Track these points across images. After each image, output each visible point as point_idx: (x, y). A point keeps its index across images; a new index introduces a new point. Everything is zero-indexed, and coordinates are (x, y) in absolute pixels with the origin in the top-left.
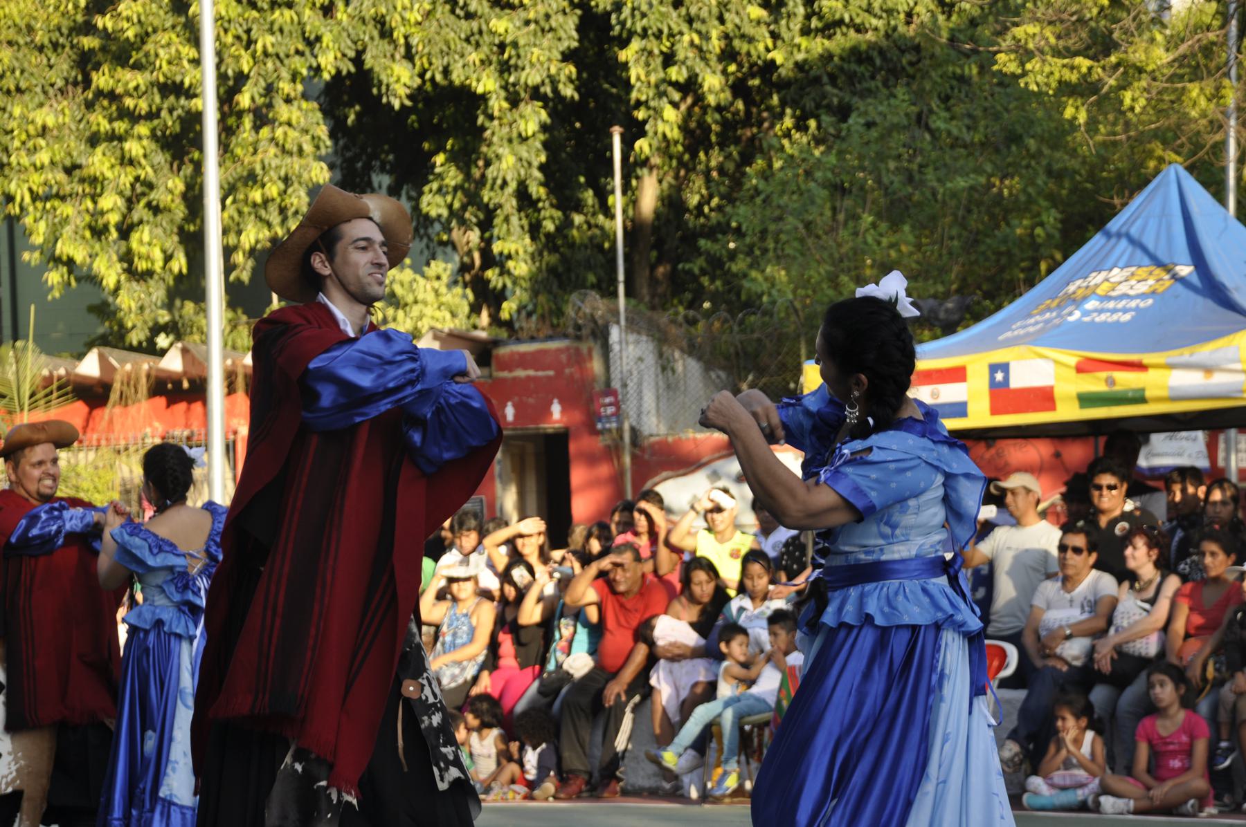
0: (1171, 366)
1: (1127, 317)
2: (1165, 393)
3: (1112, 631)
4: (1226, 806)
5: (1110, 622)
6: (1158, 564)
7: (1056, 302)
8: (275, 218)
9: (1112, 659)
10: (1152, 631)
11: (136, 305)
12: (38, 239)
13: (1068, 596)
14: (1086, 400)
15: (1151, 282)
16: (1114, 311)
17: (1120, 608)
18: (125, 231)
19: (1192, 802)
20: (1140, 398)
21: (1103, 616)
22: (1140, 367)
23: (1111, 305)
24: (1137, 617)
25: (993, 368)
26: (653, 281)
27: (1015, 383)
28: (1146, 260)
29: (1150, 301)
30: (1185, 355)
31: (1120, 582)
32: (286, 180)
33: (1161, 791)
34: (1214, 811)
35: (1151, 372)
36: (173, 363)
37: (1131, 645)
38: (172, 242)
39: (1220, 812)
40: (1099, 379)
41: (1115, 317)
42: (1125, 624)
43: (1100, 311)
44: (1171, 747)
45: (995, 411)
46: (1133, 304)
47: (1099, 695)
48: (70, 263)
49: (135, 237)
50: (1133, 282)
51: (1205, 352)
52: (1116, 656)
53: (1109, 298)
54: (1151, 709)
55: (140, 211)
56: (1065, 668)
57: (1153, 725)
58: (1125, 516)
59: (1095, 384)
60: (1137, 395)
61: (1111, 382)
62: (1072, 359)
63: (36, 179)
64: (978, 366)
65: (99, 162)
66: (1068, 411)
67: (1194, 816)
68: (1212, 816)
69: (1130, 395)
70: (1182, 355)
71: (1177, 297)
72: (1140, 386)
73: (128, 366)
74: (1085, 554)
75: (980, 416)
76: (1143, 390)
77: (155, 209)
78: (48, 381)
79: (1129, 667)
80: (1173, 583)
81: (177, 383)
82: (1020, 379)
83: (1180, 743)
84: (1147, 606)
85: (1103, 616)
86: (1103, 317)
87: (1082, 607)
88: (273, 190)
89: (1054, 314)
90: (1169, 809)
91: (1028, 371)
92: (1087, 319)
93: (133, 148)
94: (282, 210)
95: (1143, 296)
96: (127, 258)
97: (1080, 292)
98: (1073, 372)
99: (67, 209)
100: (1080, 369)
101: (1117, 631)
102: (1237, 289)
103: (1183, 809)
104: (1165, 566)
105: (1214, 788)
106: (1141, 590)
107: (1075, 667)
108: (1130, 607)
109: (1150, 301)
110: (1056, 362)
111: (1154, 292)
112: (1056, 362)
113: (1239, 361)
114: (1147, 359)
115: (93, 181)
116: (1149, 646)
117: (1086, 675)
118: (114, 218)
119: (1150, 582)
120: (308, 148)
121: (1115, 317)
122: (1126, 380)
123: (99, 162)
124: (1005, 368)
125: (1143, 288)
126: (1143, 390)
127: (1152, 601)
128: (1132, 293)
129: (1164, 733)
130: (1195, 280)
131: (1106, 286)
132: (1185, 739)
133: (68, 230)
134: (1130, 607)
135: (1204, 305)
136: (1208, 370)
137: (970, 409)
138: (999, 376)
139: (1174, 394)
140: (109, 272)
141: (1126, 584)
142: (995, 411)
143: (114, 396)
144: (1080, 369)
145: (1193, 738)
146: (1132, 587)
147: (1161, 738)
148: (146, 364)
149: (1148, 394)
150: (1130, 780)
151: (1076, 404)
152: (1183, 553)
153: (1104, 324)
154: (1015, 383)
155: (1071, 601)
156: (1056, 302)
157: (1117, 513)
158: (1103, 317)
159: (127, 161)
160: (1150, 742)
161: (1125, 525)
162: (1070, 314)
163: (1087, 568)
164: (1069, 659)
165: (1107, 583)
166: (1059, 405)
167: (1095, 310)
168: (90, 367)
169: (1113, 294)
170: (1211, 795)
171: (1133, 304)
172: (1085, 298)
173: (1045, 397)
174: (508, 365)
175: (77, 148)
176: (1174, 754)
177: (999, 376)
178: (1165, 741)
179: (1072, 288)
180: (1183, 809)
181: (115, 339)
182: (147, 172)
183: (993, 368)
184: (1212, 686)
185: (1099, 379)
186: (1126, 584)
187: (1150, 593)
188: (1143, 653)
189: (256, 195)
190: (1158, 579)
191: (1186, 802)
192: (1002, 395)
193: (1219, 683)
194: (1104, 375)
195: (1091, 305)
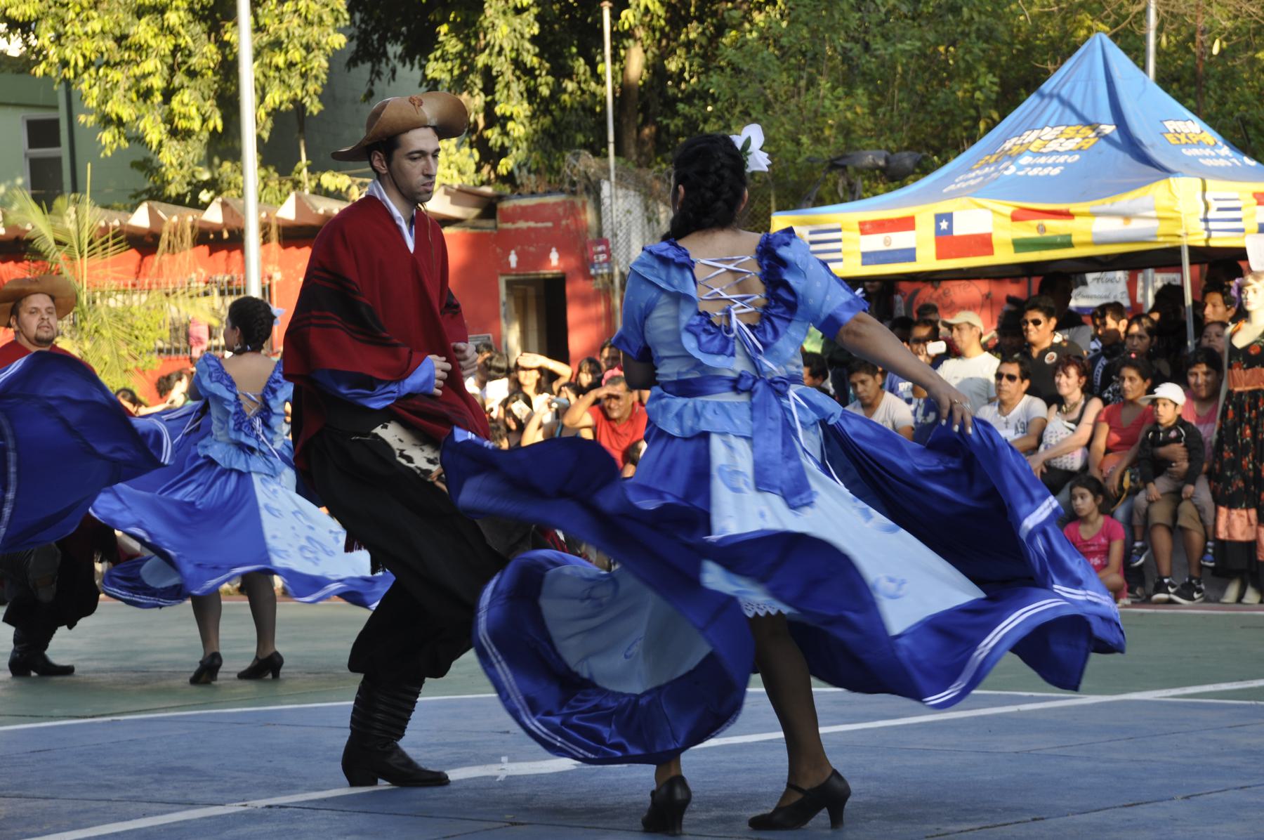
0: (1095, 214)
1: (1056, 171)
2: (1088, 238)
3: (1042, 448)
6: (1084, 390)
7: (995, 157)
8: (295, 81)
10: (1078, 447)
11: (179, 162)
12: (92, 103)
13: (1004, 419)
14: (1020, 245)
15: (1078, 139)
16: (1045, 166)
17: (1049, 428)
18: (168, 94)
20: (1069, 244)
22: (1067, 215)
23: (1043, 160)
24: (1064, 436)
25: (939, 218)
26: (640, 143)
27: (957, 232)
28: (1075, 120)
29: (1077, 157)
31: (1049, 406)
32: (308, 48)
34: (1127, 601)
35: (1077, 219)
36: (214, 215)
38: (209, 106)
40: (1031, 226)
41: (1046, 171)
42: (1053, 442)
43: (1033, 166)
44: (1092, 548)
45: (940, 256)
46: (1062, 159)
48: (120, 122)
49: (175, 103)
50: (1062, 140)
51: (1124, 201)
53: (1042, 154)
55: (180, 78)
57: (1077, 530)
58: (1054, 347)
59: (1028, 230)
60: (1065, 240)
61: (1042, 229)
62: (1008, 208)
63: (89, 46)
64: (925, 216)
65: (143, 31)
66: (1004, 255)
68: (1126, 606)
71: (1100, 153)
72: (1068, 232)
73: (177, 219)
74: (1018, 380)
75: (927, 261)
76: (1070, 236)
77: (192, 74)
78: (105, 230)
80: (1096, 405)
81: (218, 234)
82: (962, 228)
84: (1072, 426)
86: (1035, 171)
87: (1016, 428)
88: (296, 55)
91: (972, 218)
92: (1021, 173)
93: (172, 18)
94: (304, 75)
95: (1070, 152)
96: (169, 119)
97: (1015, 149)
99: (116, 75)
100: (1015, 218)
101: (1046, 448)
102: (1152, 146)
104: (1089, 391)
106: (1066, 413)
108: (1058, 427)
109: (1077, 157)
110: (993, 211)
111: (1080, 149)
112: (993, 211)
113: (1154, 209)
114: (1073, 208)
115: (139, 48)
116: (1075, 461)
118: (157, 82)
119: (1075, 405)
120: (329, 20)
121: (1046, 171)
122: (1055, 227)
123: (143, 31)
124: (949, 217)
125: (1071, 145)
126: (1070, 236)
127: (1077, 422)
128: (1061, 149)
129: (1085, 536)
130: (1117, 137)
132: (1103, 541)
133: (118, 94)
134: (1058, 427)
136: (1127, 217)
138: (944, 225)
139: (1097, 239)
140: (154, 132)
141: (1055, 407)
142: (940, 256)
143: (163, 245)
144: (1015, 218)
145: (1110, 540)
146: (1059, 409)
148: (190, 216)
149: (1074, 239)
151: (1012, 248)
152: (1107, 380)
153: (1037, 177)
154: (957, 232)
155: (1007, 423)
156: (995, 157)
157: (1047, 344)
159: (167, 30)
161: (1054, 354)
162: (1006, 169)
163: (1020, 394)
167: (1029, 165)
168: (140, 219)
169: (1044, 150)
171: (1062, 159)
172: (1020, 154)
173: (983, 243)
174: (511, 217)
175: (124, 17)
179: (1008, 145)
181: (157, 194)
182: (186, 40)
183: (939, 218)
184: (1128, 495)
185: (1031, 226)
186: (1055, 407)
187: (1075, 415)
189: (280, 60)
190: (1083, 402)
192: (946, 242)
193: (1134, 492)
194: (1036, 222)
195: (1026, 160)
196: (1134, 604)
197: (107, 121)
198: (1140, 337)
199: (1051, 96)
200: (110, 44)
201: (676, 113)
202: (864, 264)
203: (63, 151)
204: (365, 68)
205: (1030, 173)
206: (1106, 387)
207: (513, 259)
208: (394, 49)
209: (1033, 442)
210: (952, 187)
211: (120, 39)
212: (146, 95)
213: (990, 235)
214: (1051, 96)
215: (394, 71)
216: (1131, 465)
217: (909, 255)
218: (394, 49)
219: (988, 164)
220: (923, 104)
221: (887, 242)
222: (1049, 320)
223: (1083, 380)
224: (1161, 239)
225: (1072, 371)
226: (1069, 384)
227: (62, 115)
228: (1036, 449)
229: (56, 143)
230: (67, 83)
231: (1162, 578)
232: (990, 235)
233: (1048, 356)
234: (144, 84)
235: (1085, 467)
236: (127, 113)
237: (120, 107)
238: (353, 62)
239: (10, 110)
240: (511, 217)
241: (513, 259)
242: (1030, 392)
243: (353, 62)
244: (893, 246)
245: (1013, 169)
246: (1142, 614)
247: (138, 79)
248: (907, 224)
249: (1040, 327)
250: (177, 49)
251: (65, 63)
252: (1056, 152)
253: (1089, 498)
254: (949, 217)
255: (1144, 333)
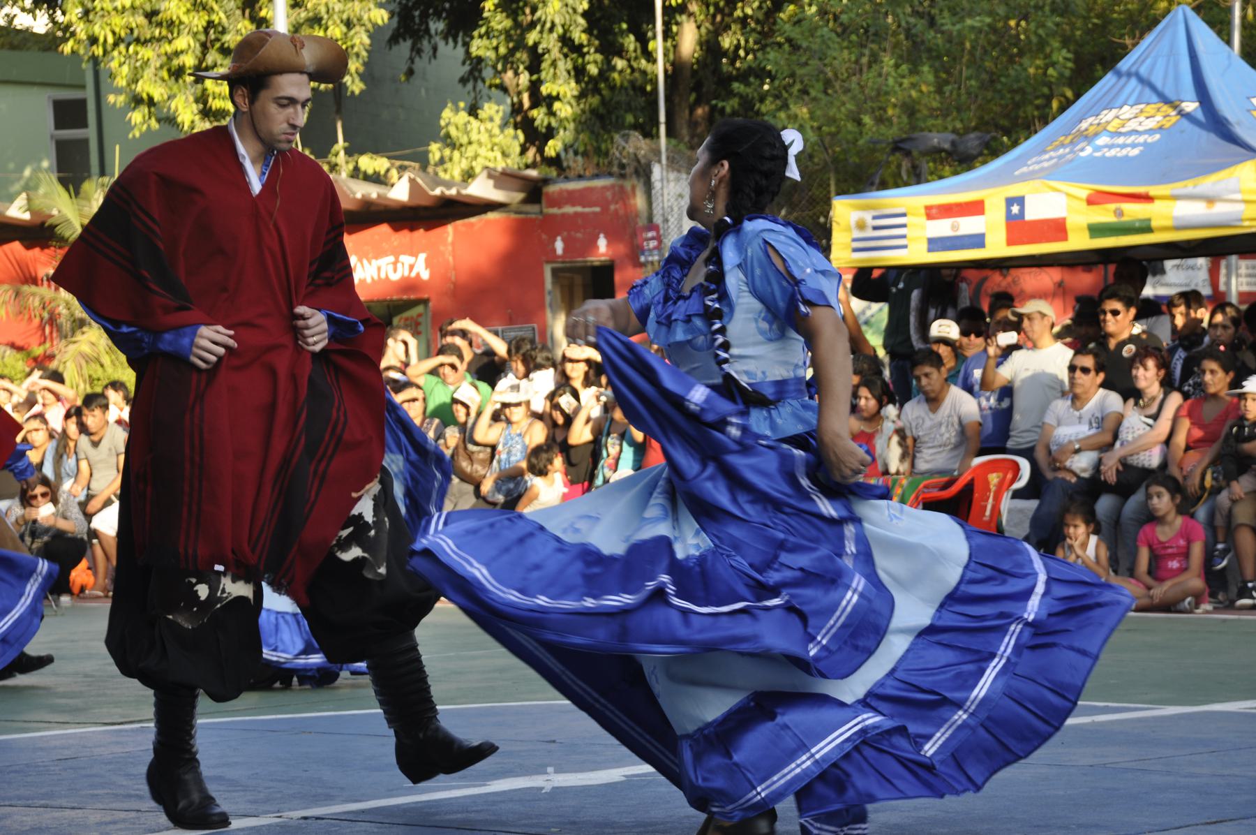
1: (1136, 152)
2: (1169, 223)
3: (1118, 444)
4: (1220, 602)
5: (1116, 436)
9: (1117, 470)
12: (121, 82)
13: (1077, 413)
14: (1096, 230)
15: (1159, 118)
16: (1123, 146)
17: (1126, 423)
19: (1189, 599)
21: (1110, 431)
22: (1147, 198)
23: (1121, 140)
24: (1141, 432)
25: (1010, 202)
26: (693, 124)
27: (1029, 216)
28: (1154, 98)
29: (1157, 136)
30: (1188, 186)
31: (1125, 400)
32: (349, 24)
33: (1161, 591)
34: (1207, 607)
35: (1157, 203)
37: (1135, 457)
39: (1215, 608)
40: (1107, 210)
41: (1124, 152)
42: (1130, 438)
43: (1110, 147)
44: (1170, 551)
45: (1011, 242)
46: (1141, 139)
47: (1104, 504)
48: (151, 102)
50: (1142, 118)
51: (1207, 184)
52: (1121, 468)
53: (1120, 134)
54: (1151, 518)
56: (1074, 480)
57: (1154, 531)
58: (1133, 339)
59: (1104, 214)
60: (1144, 225)
61: (1119, 213)
62: (1083, 191)
63: (118, 22)
64: (995, 200)
66: (1078, 241)
67: (1191, 612)
68: (1207, 612)
69: (1137, 225)
70: (1186, 186)
71: (1182, 132)
74: (1093, 373)
75: (997, 247)
76: (1149, 220)
79: (1133, 479)
80: (1175, 399)
82: (1034, 212)
83: (1178, 547)
84: (1150, 421)
85: (1110, 431)
86: (1113, 152)
87: (1090, 423)
89: (1067, 150)
90: (1168, 606)
92: (1098, 154)
95: (1150, 132)
97: (1092, 129)
98: (1084, 204)
99: (146, 53)
100: (1091, 201)
101: (1122, 444)
102: (1239, 124)
103: (1181, 606)
104: (1168, 384)
105: (1209, 587)
106: (1144, 407)
107: (1084, 479)
108: (1135, 423)
109: (1157, 136)
110: (1068, 194)
111: (1161, 128)
112: (1068, 194)
113: (1240, 192)
114: (1153, 191)
115: (171, 24)
116: (1153, 459)
117: (1093, 486)
118: (189, 61)
119: (1153, 399)
121: (1124, 152)
122: (1134, 211)
124: (1020, 201)
125: (1151, 124)
126: (1149, 220)
127: (1155, 417)
128: (1140, 129)
129: (1163, 538)
131: (1116, 123)
132: (1182, 542)
133: (148, 73)
134: (1135, 423)
135: (1208, 139)
136: (1210, 200)
137: (988, 240)
138: (1015, 209)
144: (1091, 201)
145: (1189, 542)
146: (1136, 404)
147: (1161, 543)
149: (1154, 224)
150: (1133, 581)
151: (1087, 234)
153: (1115, 157)
154: (1029, 216)
155: (1080, 418)
156: (1068, 140)
157: (1125, 336)
158: (1113, 152)
160: (1150, 547)
162: (1082, 150)
164: (1078, 472)
165: (1114, 400)
166: (1070, 235)
169: (1123, 130)
170: (1206, 594)
171: (1141, 139)
172: (1096, 135)
173: (1057, 228)
174: (557, 202)
176: (1172, 556)
177: (1015, 209)
178: (1164, 546)
179: (1084, 125)
180: (1181, 606)
183: (1010, 202)
184: (1210, 494)
185: (1107, 210)
186: (1131, 402)
187: (1153, 409)
188: (1147, 464)
190: (1161, 396)
191: (1183, 600)
192: (1018, 227)
193: (1216, 491)
194: (1112, 206)
195: (1101, 141)
196: (1216, 610)
197: (137, 101)
198: (1225, 327)
199: (1129, 75)
200: (141, 20)
201: (731, 94)
202: (930, 250)
203: (91, 132)
204: (405, 47)
205: (1108, 154)
206: (1187, 380)
207: (559, 246)
208: (437, 26)
209: (1108, 438)
210: (1025, 169)
211: (151, 15)
212: (178, 73)
213: (1064, 220)
214: (1129, 75)
215: (435, 49)
216: (1213, 463)
217: (978, 241)
218: (437, 26)
219: (1063, 145)
220: (992, 82)
221: (954, 228)
222: (1128, 311)
223: (1162, 372)
224: (1246, 223)
225: (1151, 363)
226: (1147, 377)
227: (89, 94)
228: (1111, 446)
229: (84, 124)
230: (95, 60)
231: (1245, 582)
232: (1064, 220)
233: (1126, 348)
234: (175, 62)
235: (1164, 465)
236: (158, 93)
237: (151, 87)
238: (395, 39)
239: (35, 90)
240: (557, 202)
241: (559, 246)
242: (1105, 385)
243: (395, 39)
244: (962, 232)
245: (1089, 150)
246: (1225, 621)
247: (170, 57)
248: (976, 208)
249: (1119, 317)
250: (210, 24)
251: (93, 40)
252: (1135, 132)
253: (1166, 497)
254: (1020, 201)
255: (1228, 323)
